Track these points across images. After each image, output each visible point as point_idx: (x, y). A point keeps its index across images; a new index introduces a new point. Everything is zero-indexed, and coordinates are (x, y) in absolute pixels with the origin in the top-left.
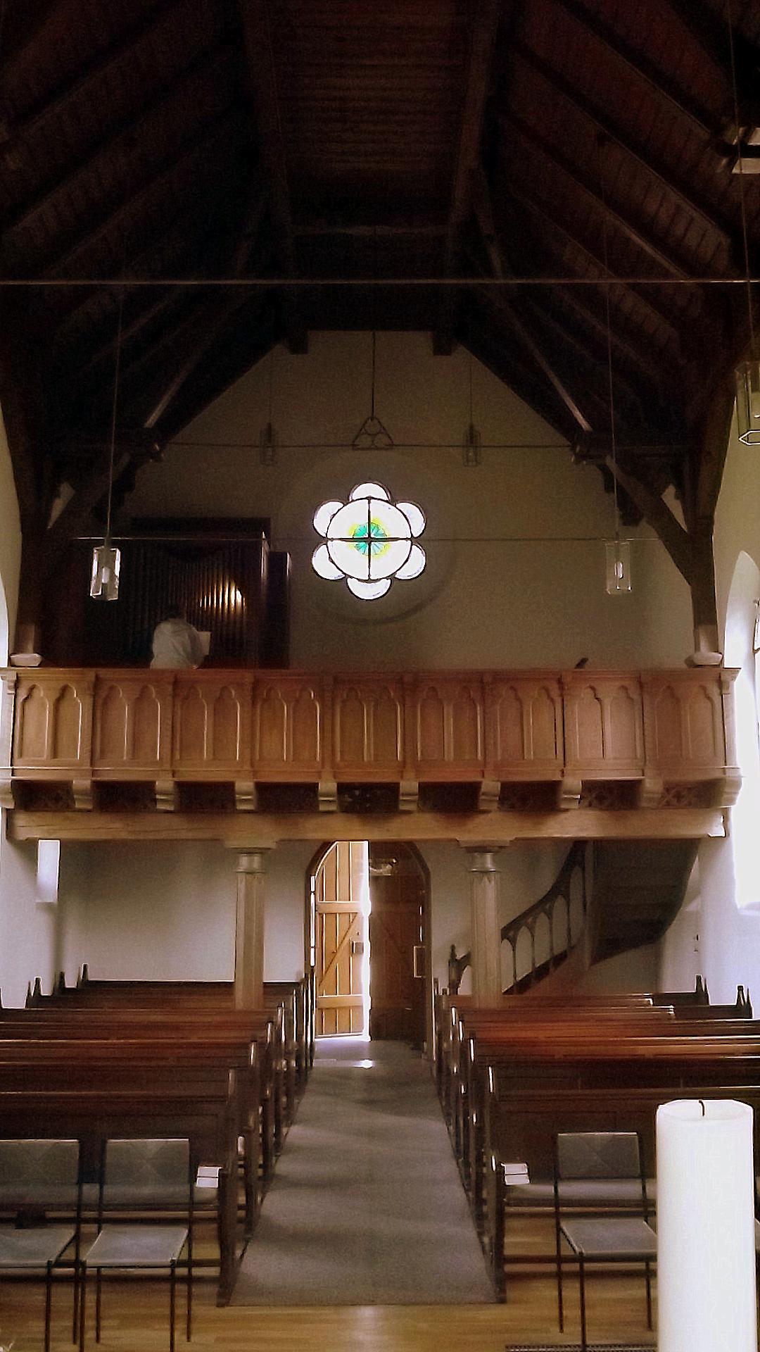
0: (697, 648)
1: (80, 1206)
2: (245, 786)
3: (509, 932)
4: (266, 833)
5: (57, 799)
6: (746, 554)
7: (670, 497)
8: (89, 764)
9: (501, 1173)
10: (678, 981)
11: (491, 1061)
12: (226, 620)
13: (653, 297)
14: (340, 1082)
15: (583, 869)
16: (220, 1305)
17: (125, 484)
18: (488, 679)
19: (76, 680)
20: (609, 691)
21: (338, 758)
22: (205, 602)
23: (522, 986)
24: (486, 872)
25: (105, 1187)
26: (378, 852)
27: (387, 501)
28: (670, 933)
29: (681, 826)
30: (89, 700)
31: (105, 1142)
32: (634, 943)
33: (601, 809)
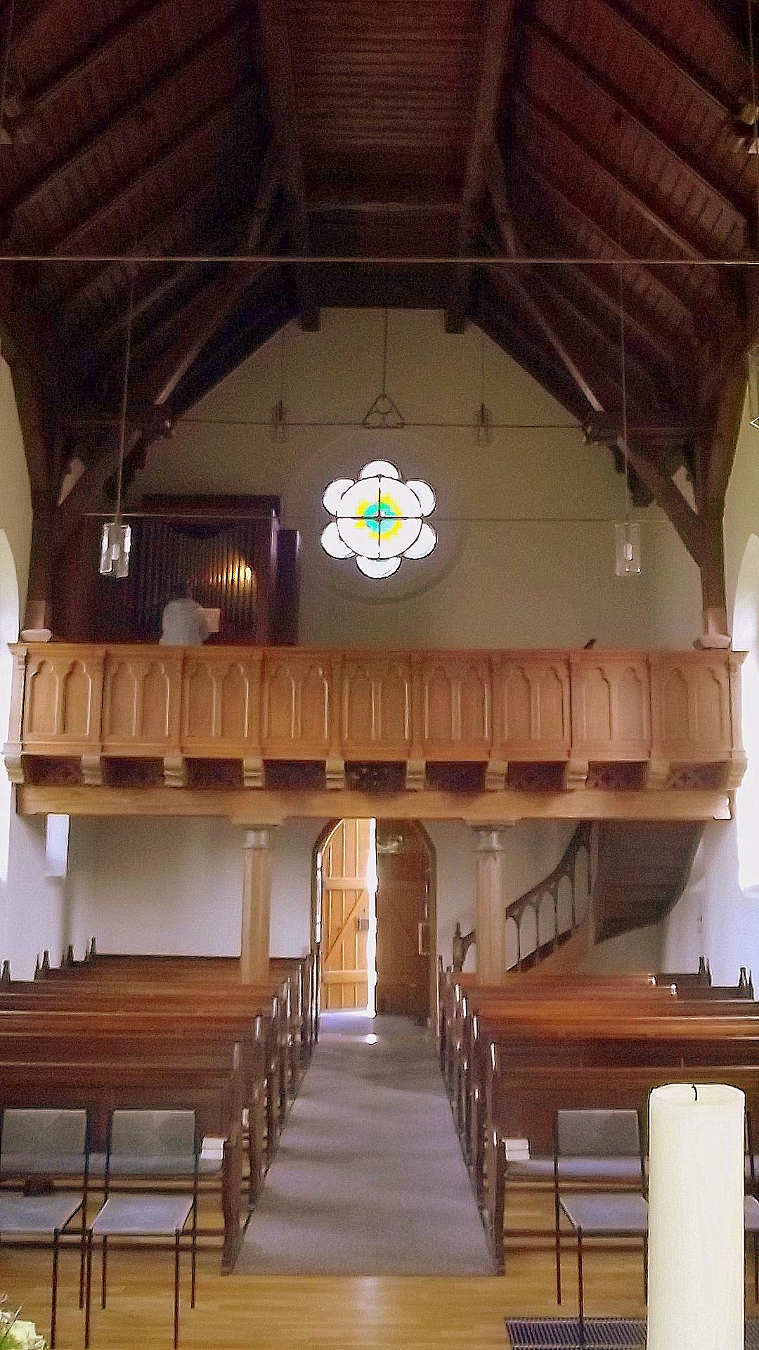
0: (706, 630)
2: (252, 763)
3: (514, 911)
7: (680, 478)
9: (502, 1148)
10: (680, 961)
12: (241, 593)
14: (345, 1056)
16: (224, 1274)
17: (136, 459)
18: (496, 659)
19: (87, 655)
20: (616, 674)
23: (526, 964)
26: (386, 830)
28: (675, 914)
29: (685, 807)
30: (99, 676)
32: (639, 922)
33: (606, 789)
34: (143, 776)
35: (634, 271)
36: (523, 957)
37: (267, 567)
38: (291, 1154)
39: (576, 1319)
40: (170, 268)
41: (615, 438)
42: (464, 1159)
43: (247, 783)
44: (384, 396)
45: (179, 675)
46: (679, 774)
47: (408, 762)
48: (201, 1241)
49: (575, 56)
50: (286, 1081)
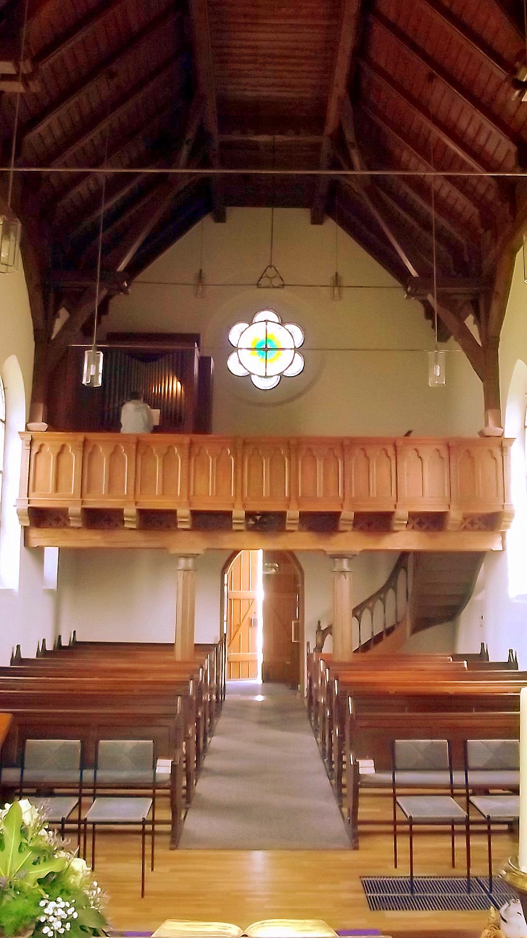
0: (487, 424)
1: (81, 785)
2: (183, 512)
3: (357, 612)
4: (197, 544)
5: (58, 520)
6: (522, 361)
7: (470, 321)
8: (80, 496)
9: (356, 766)
10: (467, 645)
11: (350, 693)
12: (174, 400)
13: (461, 184)
14: (243, 709)
15: (406, 571)
16: (172, 849)
17: (104, 308)
18: (346, 443)
19: (71, 440)
20: (428, 453)
21: (246, 494)
22: (155, 390)
23: (365, 648)
24: (343, 572)
25: (97, 771)
26: (272, 556)
27: (278, 323)
28: (464, 615)
29: (473, 542)
30: (80, 454)
31: (97, 742)
33: (420, 531)
34: (109, 520)
35: (439, 182)
36: (362, 643)
37: (192, 382)
38: (212, 772)
39: (408, 877)
40: (129, 177)
41: (426, 295)
42: (328, 774)
43: (179, 526)
44: (271, 266)
45: (134, 453)
46: (468, 521)
47: (288, 512)
48: (158, 828)
49: (401, 35)
50: (207, 725)
